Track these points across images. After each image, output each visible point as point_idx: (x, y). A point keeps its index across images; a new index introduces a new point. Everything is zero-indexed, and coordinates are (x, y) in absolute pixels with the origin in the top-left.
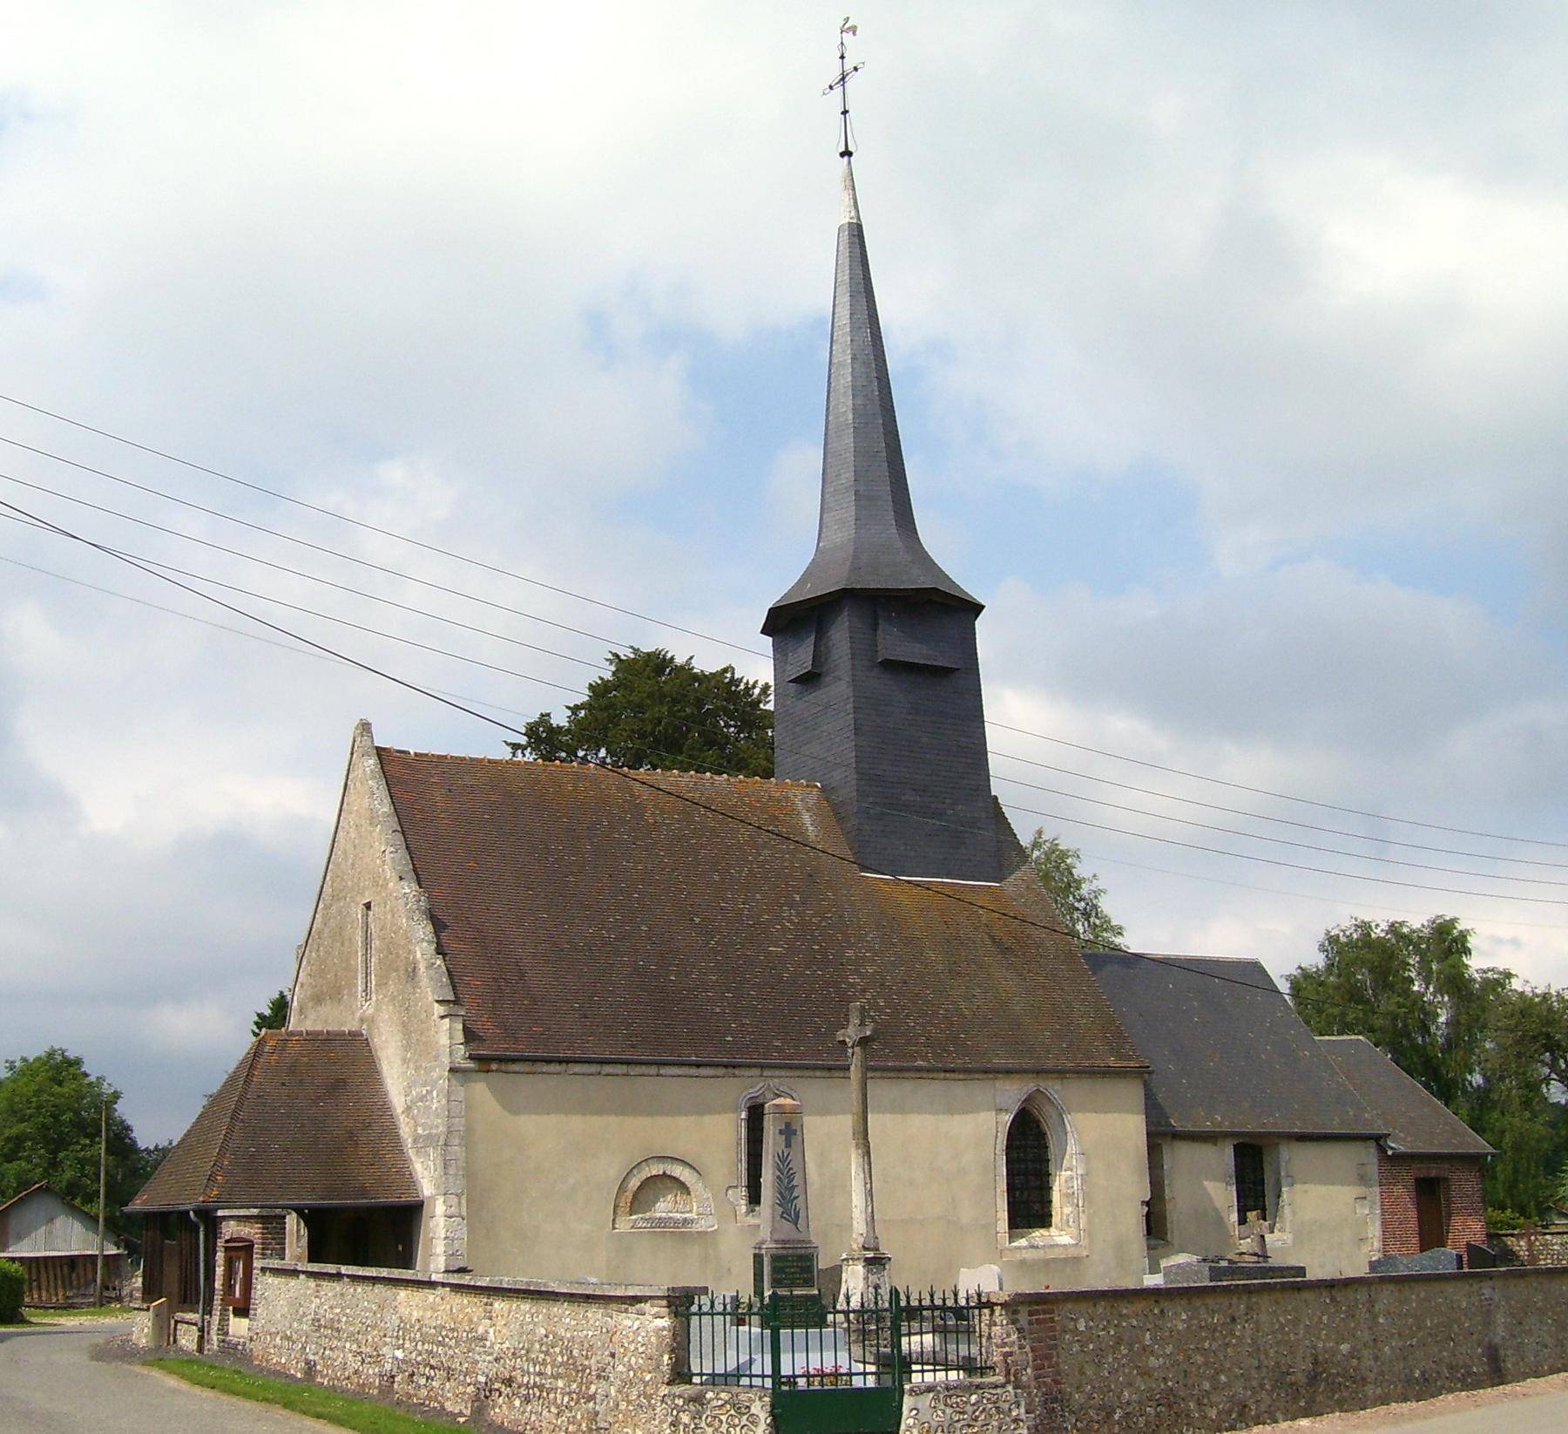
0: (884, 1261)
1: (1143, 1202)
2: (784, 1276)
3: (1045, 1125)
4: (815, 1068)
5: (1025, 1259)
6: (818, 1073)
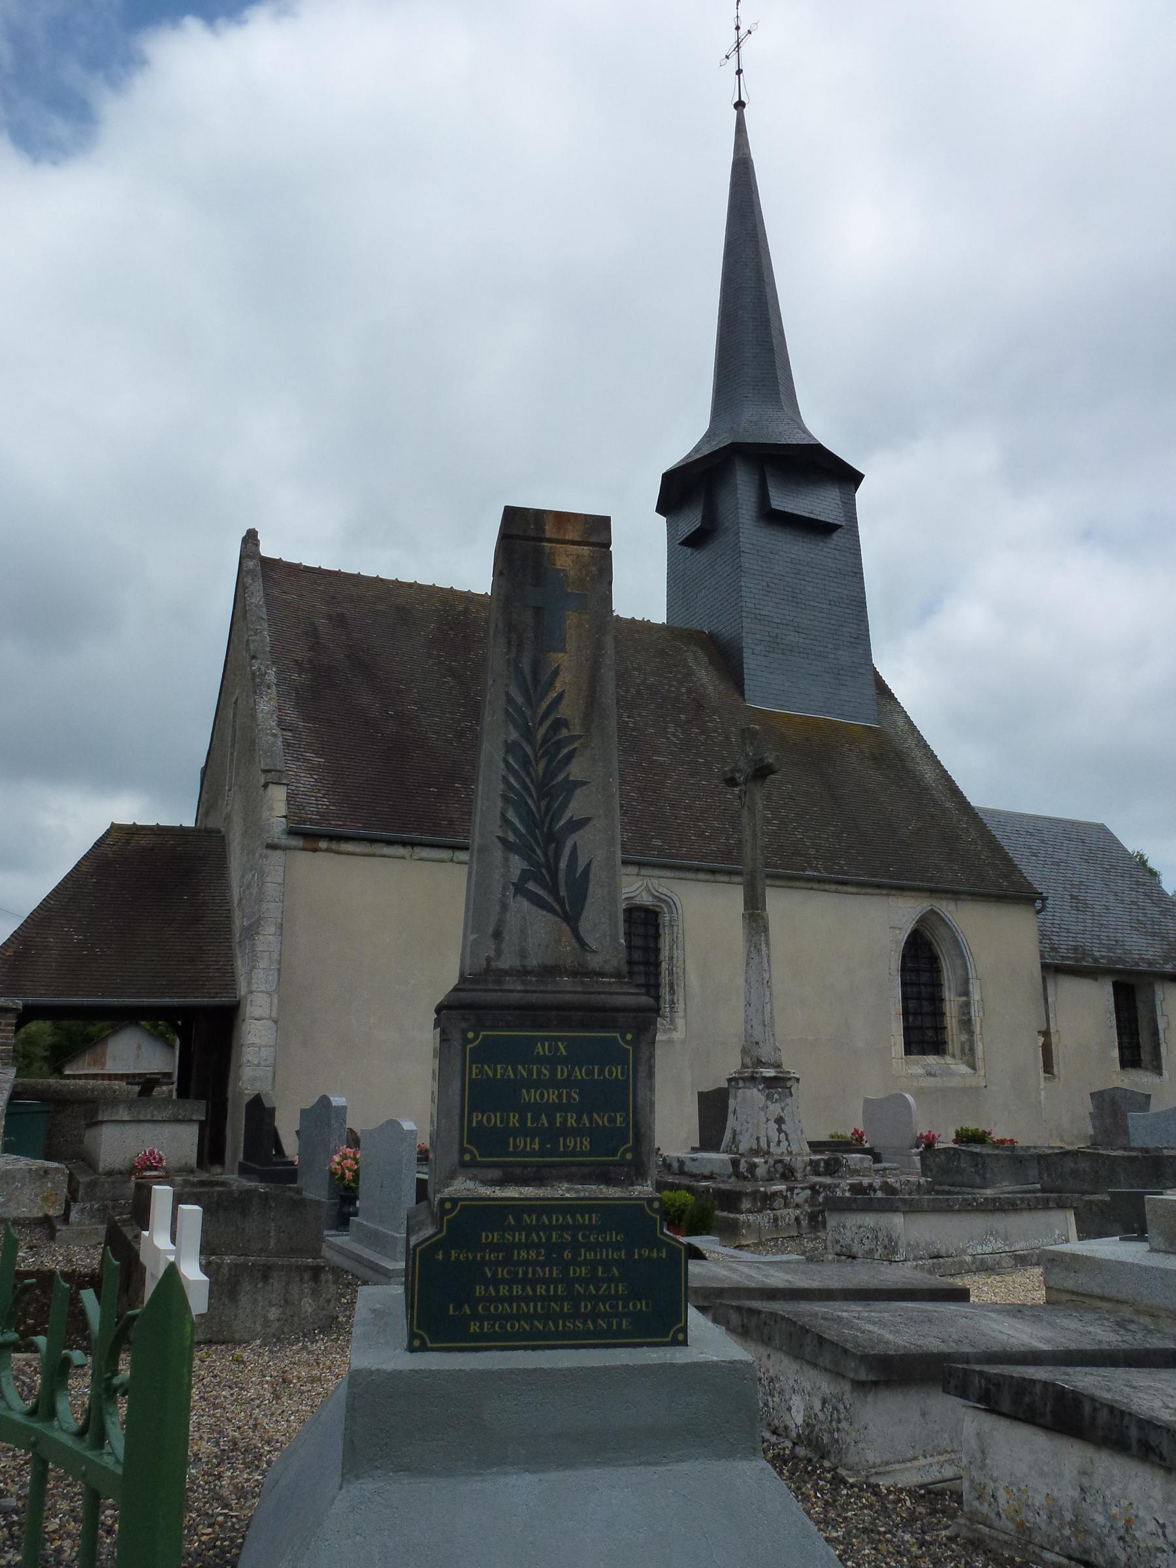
0: (789, 1084)
1: (1039, 1032)
2: (514, 1120)
3: (937, 948)
4: (698, 870)
5: (922, 1088)
6: (701, 876)
